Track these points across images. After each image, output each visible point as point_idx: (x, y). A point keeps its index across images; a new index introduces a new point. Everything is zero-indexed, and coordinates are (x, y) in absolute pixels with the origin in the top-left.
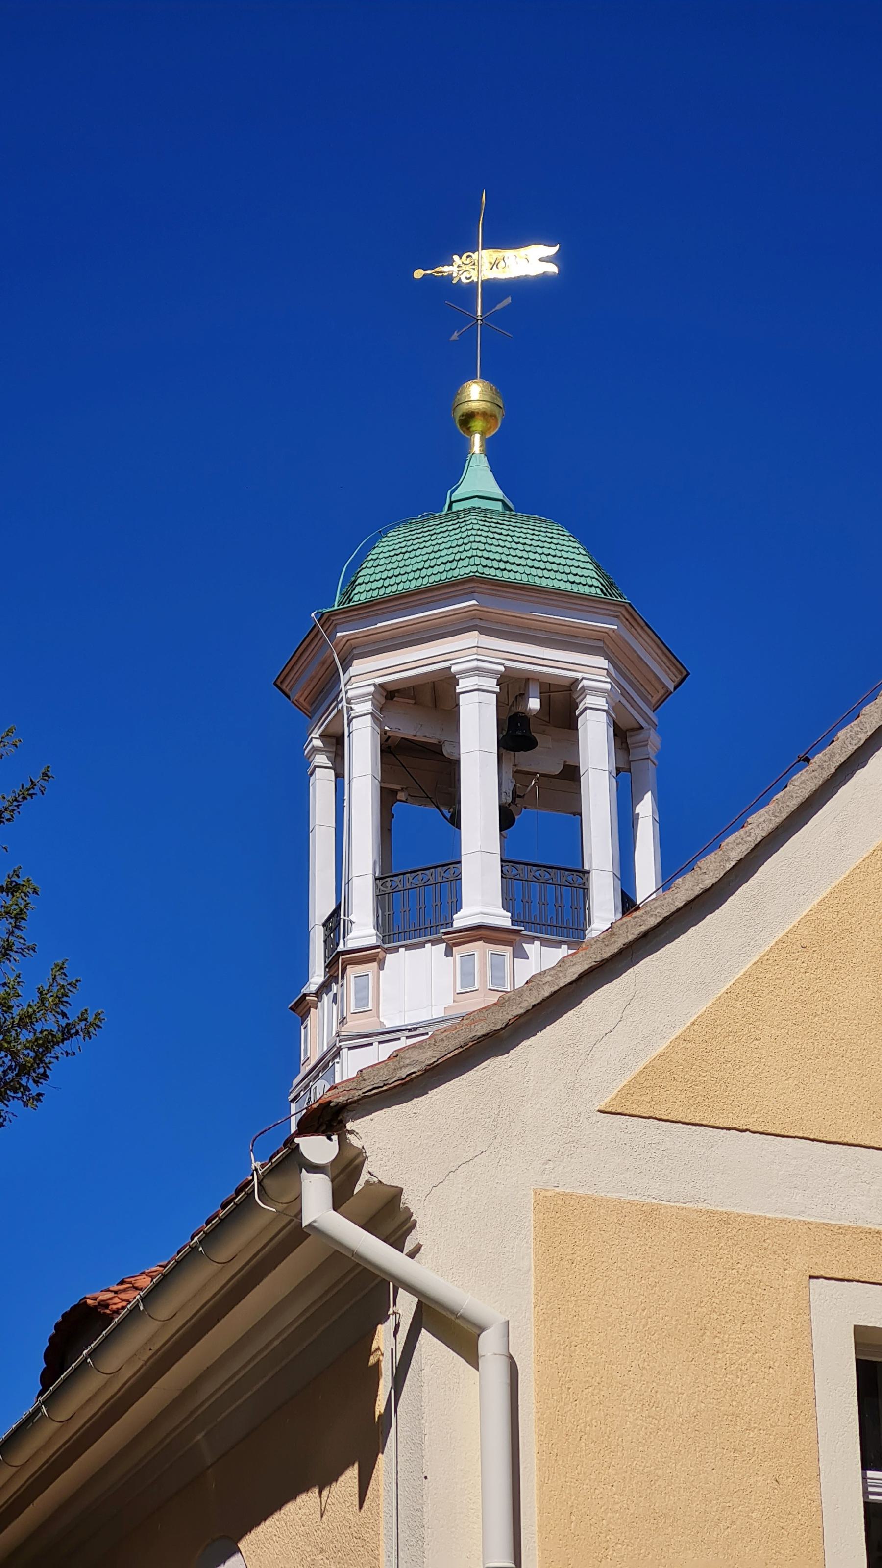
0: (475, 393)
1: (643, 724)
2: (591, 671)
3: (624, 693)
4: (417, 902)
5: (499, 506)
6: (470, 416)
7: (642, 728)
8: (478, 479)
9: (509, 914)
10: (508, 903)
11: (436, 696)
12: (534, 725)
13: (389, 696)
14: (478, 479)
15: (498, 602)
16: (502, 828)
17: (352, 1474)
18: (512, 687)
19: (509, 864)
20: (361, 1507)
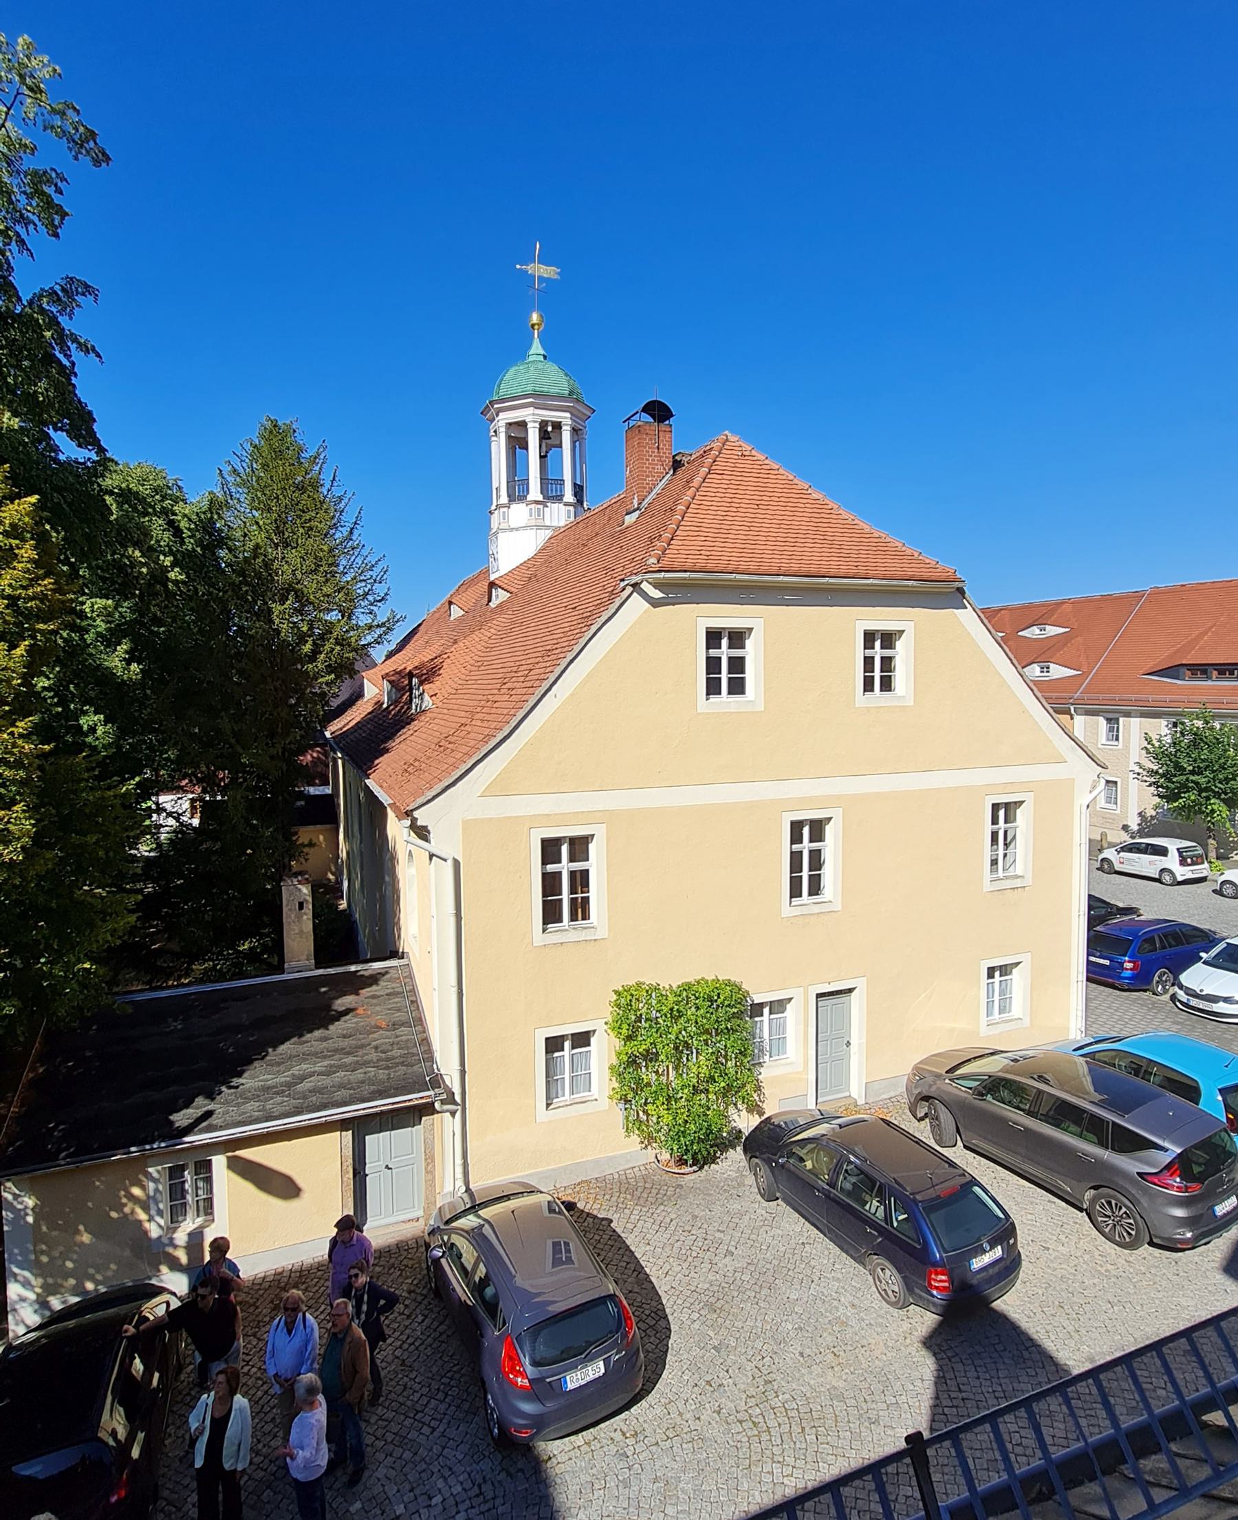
0: (535, 318)
2: (565, 418)
4: (517, 492)
5: (541, 358)
6: (533, 326)
8: (537, 348)
11: (523, 425)
12: (549, 433)
13: (510, 425)
14: (537, 348)
15: (540, 398)
18: (543, 425)
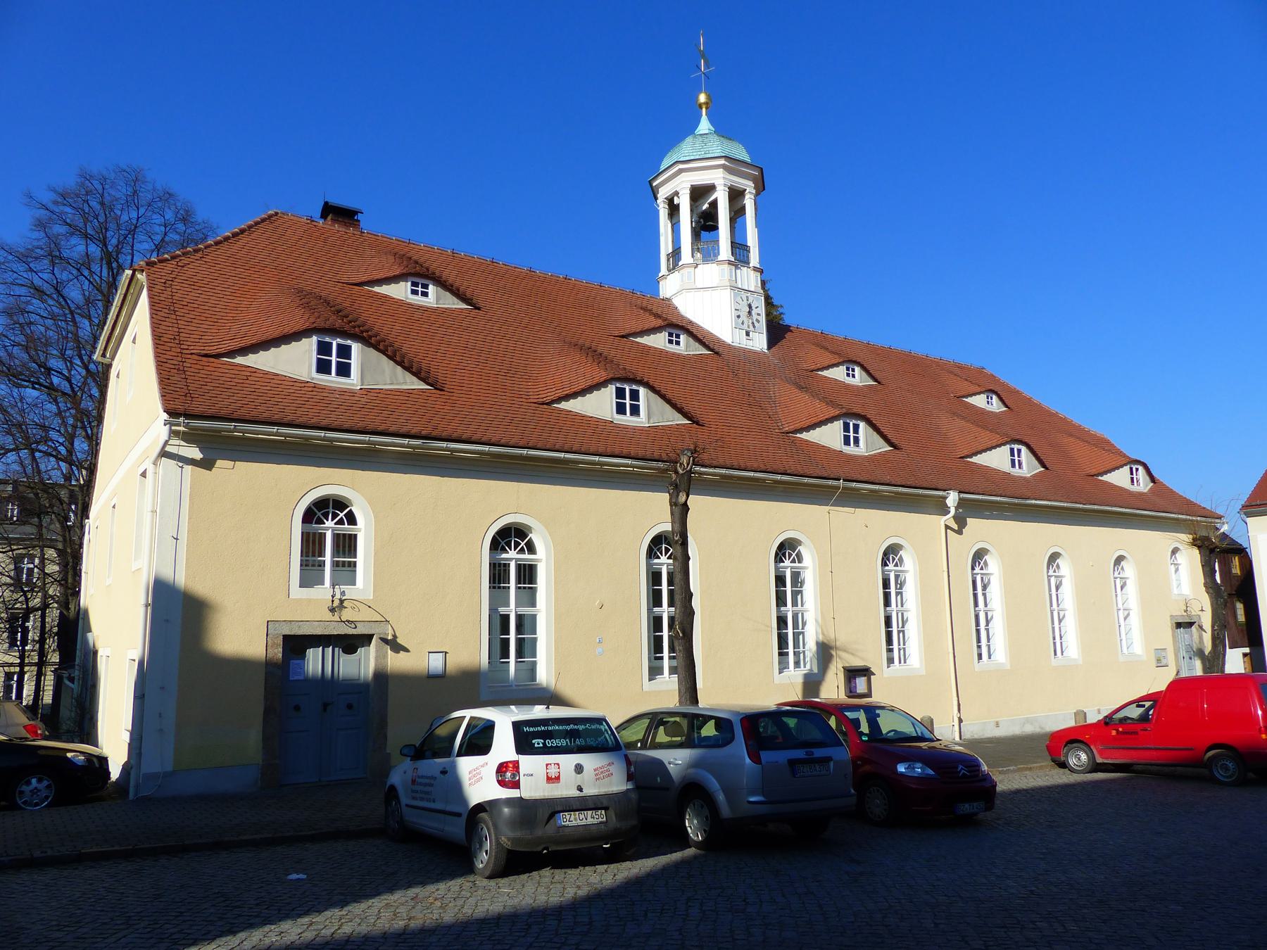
2: (749, 186)
8: (704, 126)
14: (704, 126)
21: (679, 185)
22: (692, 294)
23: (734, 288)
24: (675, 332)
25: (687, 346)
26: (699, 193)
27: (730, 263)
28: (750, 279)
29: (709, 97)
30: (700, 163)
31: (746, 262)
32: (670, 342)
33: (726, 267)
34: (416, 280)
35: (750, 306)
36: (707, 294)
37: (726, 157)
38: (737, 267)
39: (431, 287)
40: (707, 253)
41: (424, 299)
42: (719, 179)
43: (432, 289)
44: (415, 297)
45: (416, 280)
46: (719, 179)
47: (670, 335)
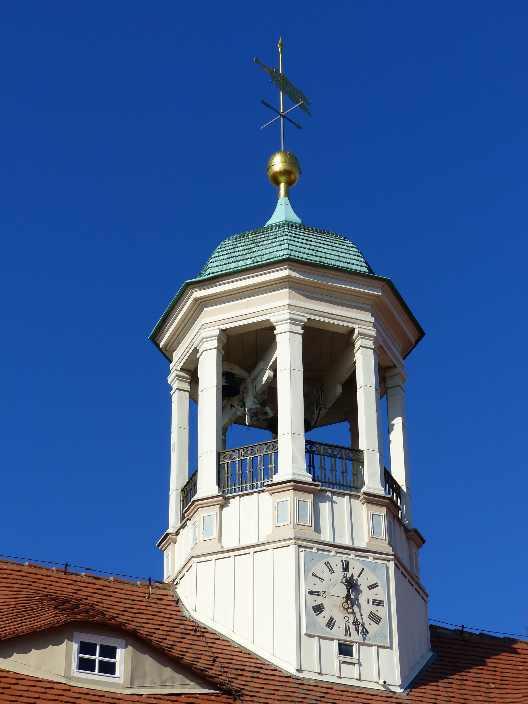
1: (396, 364)
2: (362, 323)
3: (385, 342)
7: (396, 366)
8: (283, 211)
9: (311, 476)
10: (311, 468)
12: (325, 351)
14: (283, 211)
16: (306, 431)
17: (297, 219)
19: (311, 447)
20: (309, 114)
21: (200, 336)
22: (226, 565)
23: (302, 543)
24: (99, 640)
25: (133, 676)
26: (245, 350)
27: (298, 486)
28: (355, 522)
29: (293, 160)
30: (258, 291)
31: (351, 485)
32: (85, 665)
33: (289, 497)
34: (89, 638)
35: (351, 585)
36: (244, 561)
37: (290, 262)
38: (319, 496)
39: (120, 652)
40: (244, 467)
41: (106, 678)
42: (279, 310)
43: (122, 657)
44: (86, 675)
45: (89, 638)
46: (279, 310)
47: (86, 648)
